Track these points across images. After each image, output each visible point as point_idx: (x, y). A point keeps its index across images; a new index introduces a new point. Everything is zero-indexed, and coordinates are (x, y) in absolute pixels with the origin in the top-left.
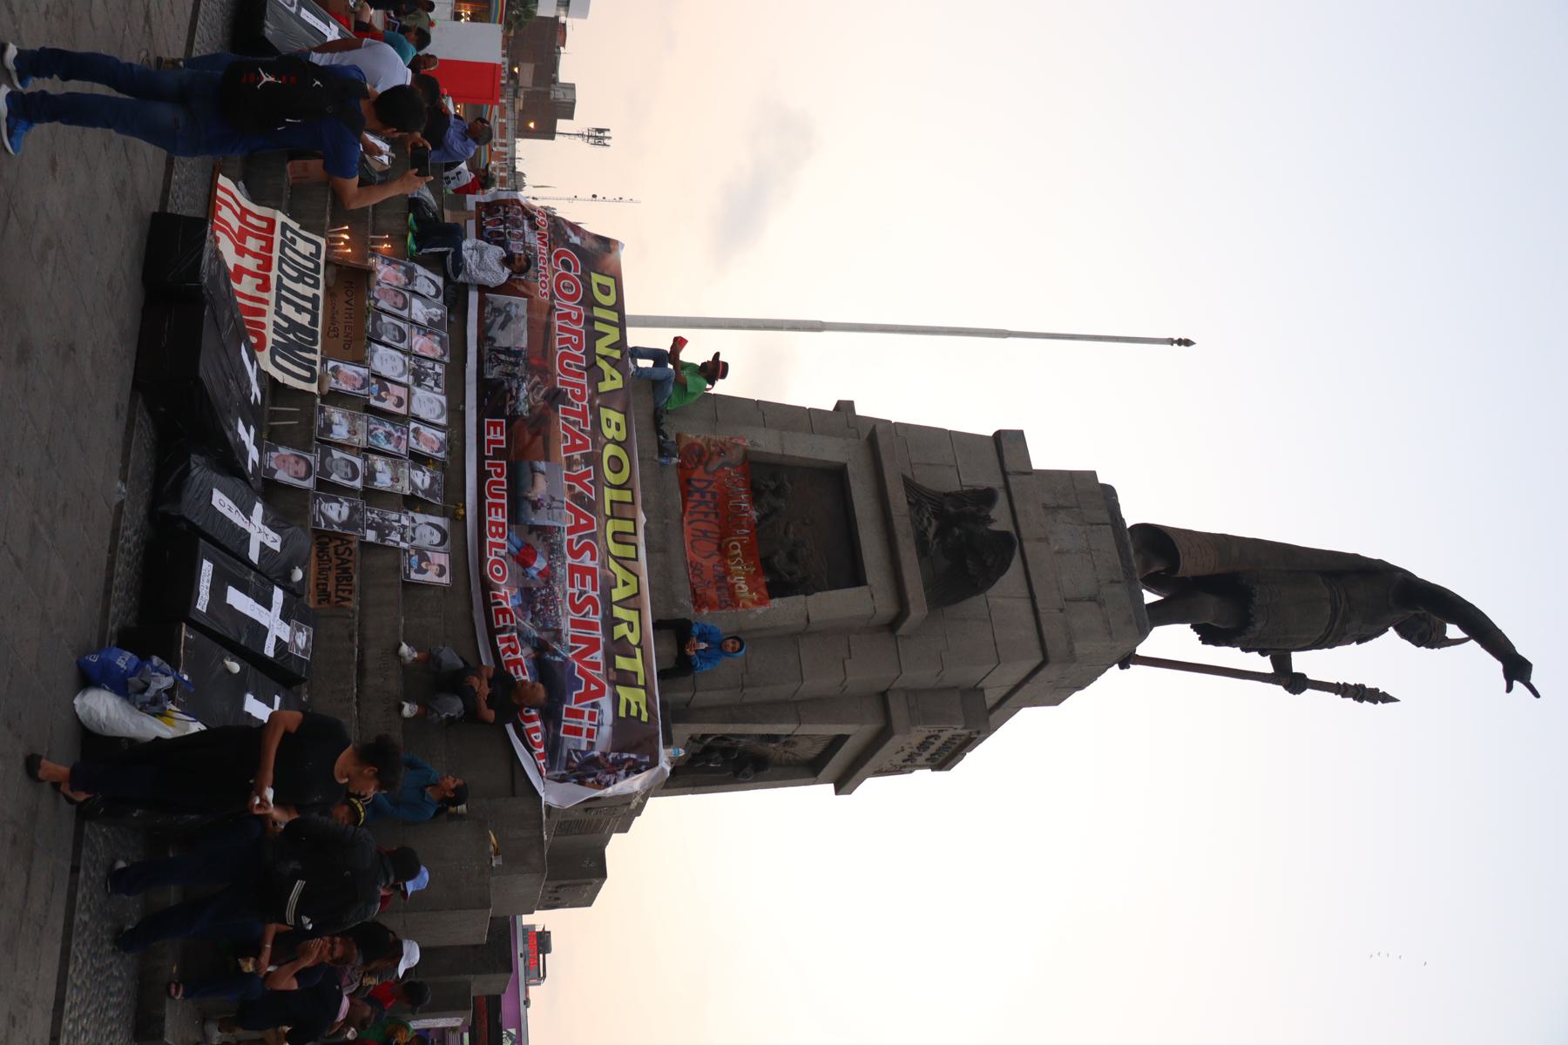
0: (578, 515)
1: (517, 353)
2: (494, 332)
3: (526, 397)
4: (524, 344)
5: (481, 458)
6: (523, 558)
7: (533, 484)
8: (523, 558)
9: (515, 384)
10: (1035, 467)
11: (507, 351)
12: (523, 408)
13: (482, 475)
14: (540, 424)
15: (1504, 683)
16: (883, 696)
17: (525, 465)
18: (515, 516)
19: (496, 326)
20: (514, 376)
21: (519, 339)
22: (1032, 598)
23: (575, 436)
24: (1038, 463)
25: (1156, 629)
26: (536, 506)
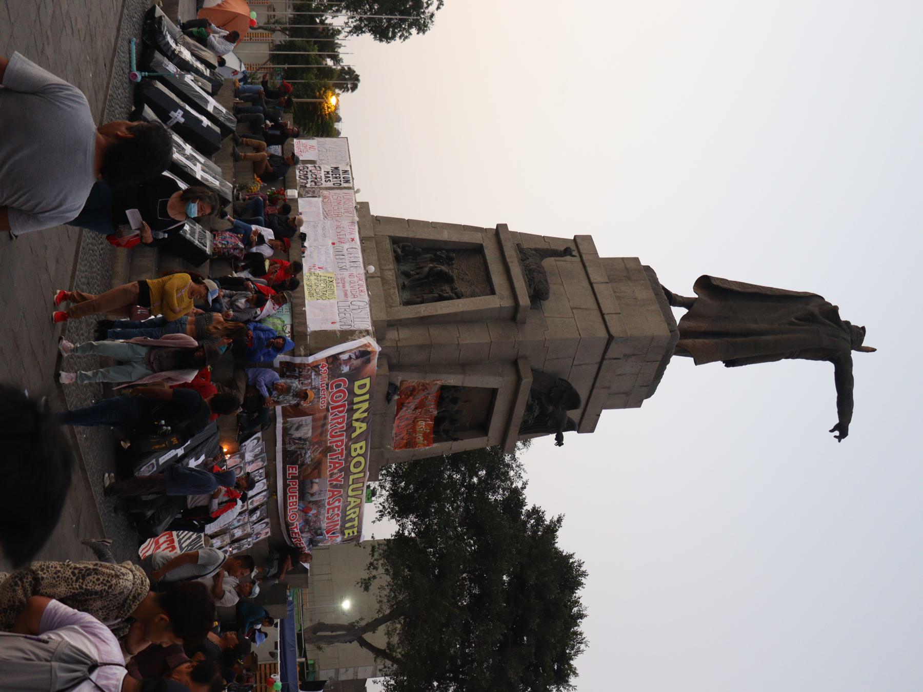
0: (333, 492)
1: (305, 440)
2: (288, 446)
3: (309, 456)
4: (310, 434)
5: (285, 479)
6: (305, 511)
7: (312, 487)
8: (305, 511)
9: (303, 452)
10: (601, 256)
11: (300, 439)
12: (308, 461)
13: (285, 486)
14: (318, 466)
15: (832, 428)
16: (515, 363)
17: (308, 481)
18: (302, 497)
19: (293, 429)
20: (303, 448)
21: (307, 433)
22: (591, 284)
23: (335, 463)
24: (601, 256)
25: (645, 401)
26: (312, 495)
